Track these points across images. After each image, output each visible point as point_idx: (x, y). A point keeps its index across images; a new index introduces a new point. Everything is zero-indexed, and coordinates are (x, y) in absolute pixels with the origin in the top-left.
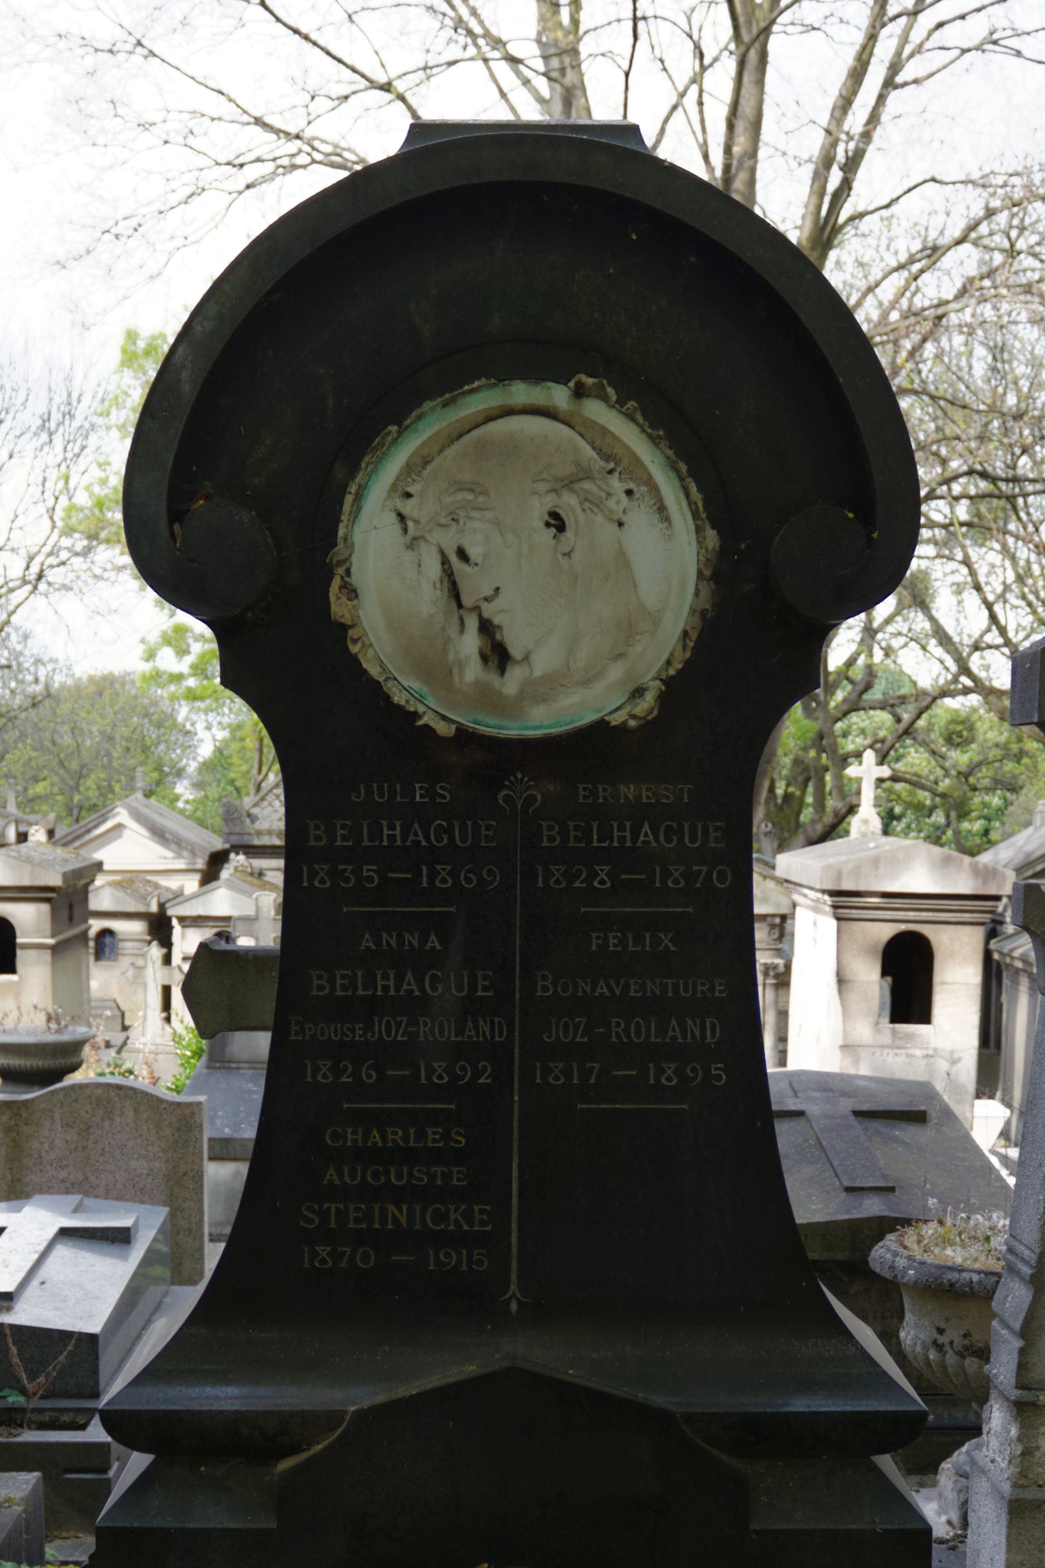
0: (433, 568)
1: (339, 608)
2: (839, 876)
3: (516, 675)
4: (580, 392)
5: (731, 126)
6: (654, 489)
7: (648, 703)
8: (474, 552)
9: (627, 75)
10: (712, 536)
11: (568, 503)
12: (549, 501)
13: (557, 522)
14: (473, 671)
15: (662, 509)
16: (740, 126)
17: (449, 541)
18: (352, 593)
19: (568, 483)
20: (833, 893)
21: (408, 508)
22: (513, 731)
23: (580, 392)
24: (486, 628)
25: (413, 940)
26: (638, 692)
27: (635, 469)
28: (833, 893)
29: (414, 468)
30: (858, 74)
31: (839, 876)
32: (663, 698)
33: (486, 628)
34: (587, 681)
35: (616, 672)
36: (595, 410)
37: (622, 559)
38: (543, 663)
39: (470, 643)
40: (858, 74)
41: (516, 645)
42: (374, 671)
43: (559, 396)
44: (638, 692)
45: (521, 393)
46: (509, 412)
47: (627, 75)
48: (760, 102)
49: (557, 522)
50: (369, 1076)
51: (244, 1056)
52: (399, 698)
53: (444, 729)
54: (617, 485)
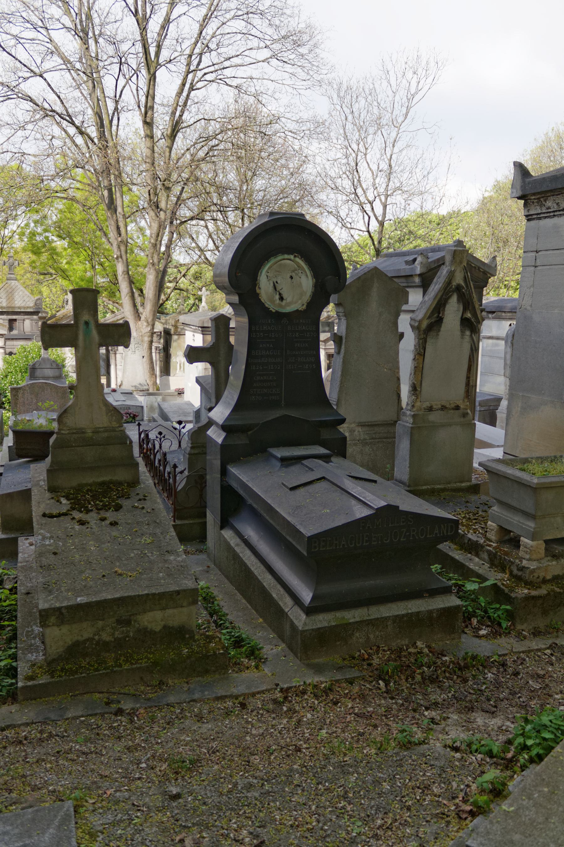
0: (272, 284)
1: (258, 291)
2: (203, 322)
3: (284, 301)
4: (295, 256)
5: (147, 97)
6: (306, 272)
7: (304, 307)
8: (279, 282)
9: (117, 81)
10: (314, 280)
11: (293, 275)
12: (291, 274)
13: (291, 277)
14: (278, 301)
15: (307, 275)
16: (149, 98)
17: (275, 280)
18: (260, 288)
19: (293, 271)
20: (202, 327)
21: (268, 274)
22: (284, 311)
23: (295, 256)
24: (280, 294)
25: (268, 345)
26: (303, 305)
27: (303, 269)
28: (202, 327)
29: (269, 268)
30: (184, 85)
31: (203, 322)
32: (307, 306)
33: (280, 294)
34: (296, 303)
35: (300, 302)
36: (297, 259)
37: (301, 283)
38: (289, 300)
39: (277, 297)
40: (184, 85)
41: (285, 296)
42: (263, 301)
43: (292, 257)
44: (303, 305)
45: (286, 256)
46: (284, 259)
47: (117, 81)
48: (154, 91)
49: (291, 277)
50: (261, 368)
51: (41, 376)
52: (267, 306)
53: (274, 311)
54: (300, 271)
